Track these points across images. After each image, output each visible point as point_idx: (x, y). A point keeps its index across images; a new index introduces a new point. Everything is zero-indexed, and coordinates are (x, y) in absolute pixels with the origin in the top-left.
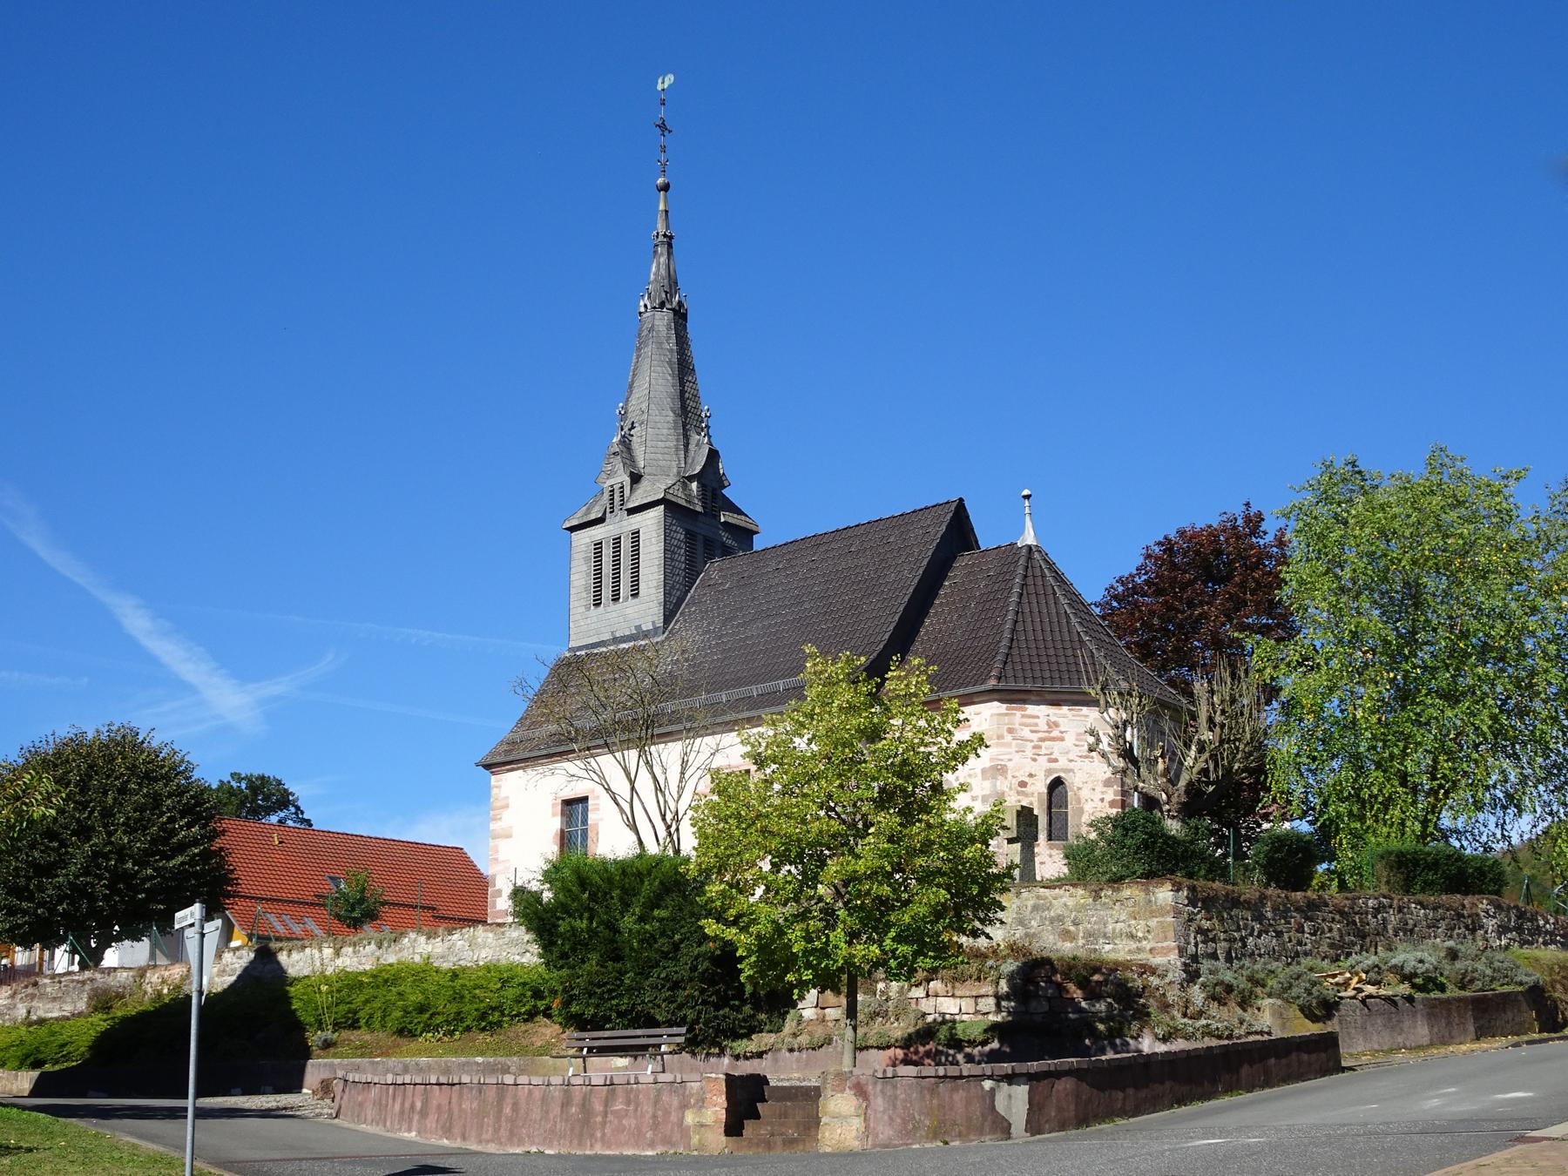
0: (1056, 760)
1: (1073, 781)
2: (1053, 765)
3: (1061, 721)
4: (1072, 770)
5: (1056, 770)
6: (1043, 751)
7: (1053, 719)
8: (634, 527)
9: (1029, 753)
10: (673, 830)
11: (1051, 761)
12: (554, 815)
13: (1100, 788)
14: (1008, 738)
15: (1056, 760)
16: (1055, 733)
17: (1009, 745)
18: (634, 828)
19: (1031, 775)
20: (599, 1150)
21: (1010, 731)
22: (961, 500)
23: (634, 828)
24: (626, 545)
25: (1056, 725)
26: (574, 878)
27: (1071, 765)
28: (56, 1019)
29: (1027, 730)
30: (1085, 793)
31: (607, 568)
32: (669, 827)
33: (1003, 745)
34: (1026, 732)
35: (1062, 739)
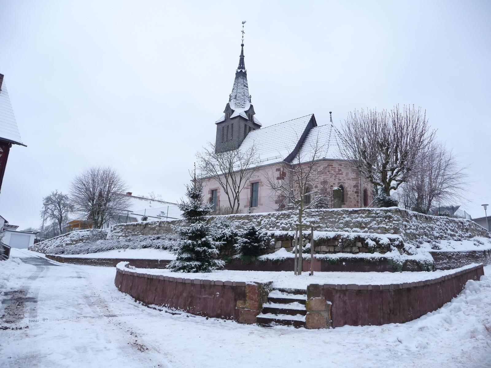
0: (341, 180)
1: (346, 185)
2: (340, 181)
3: (342, 169)
4: (345, 183)
5: (340, 183)
6: (337, 177)
7: (340, 168)
8: (232, 123)
9: (333, 177)
10: (237, 195)
11: (339, 180)
12: (209, 194)
13: (352, 188)
14: (328, 173)
15: (341, 180)
16: (340, 173)
17: (328, 175)
18: (227, 193)
19: (334, 184)
20: (227, 216)
21: (328, 171)
22: (313, 114)
23: (227, 193)
24: (230, 127)
25: (340, 170)
26: (98, 169)
27: (345, 181)
28: (98, 239)
29: (333, 171)
30: (348, 189)
31: (225, 133)
32: (236, 194)
33: (327, 175)
34: (333, 172)
35: (342, 174)
